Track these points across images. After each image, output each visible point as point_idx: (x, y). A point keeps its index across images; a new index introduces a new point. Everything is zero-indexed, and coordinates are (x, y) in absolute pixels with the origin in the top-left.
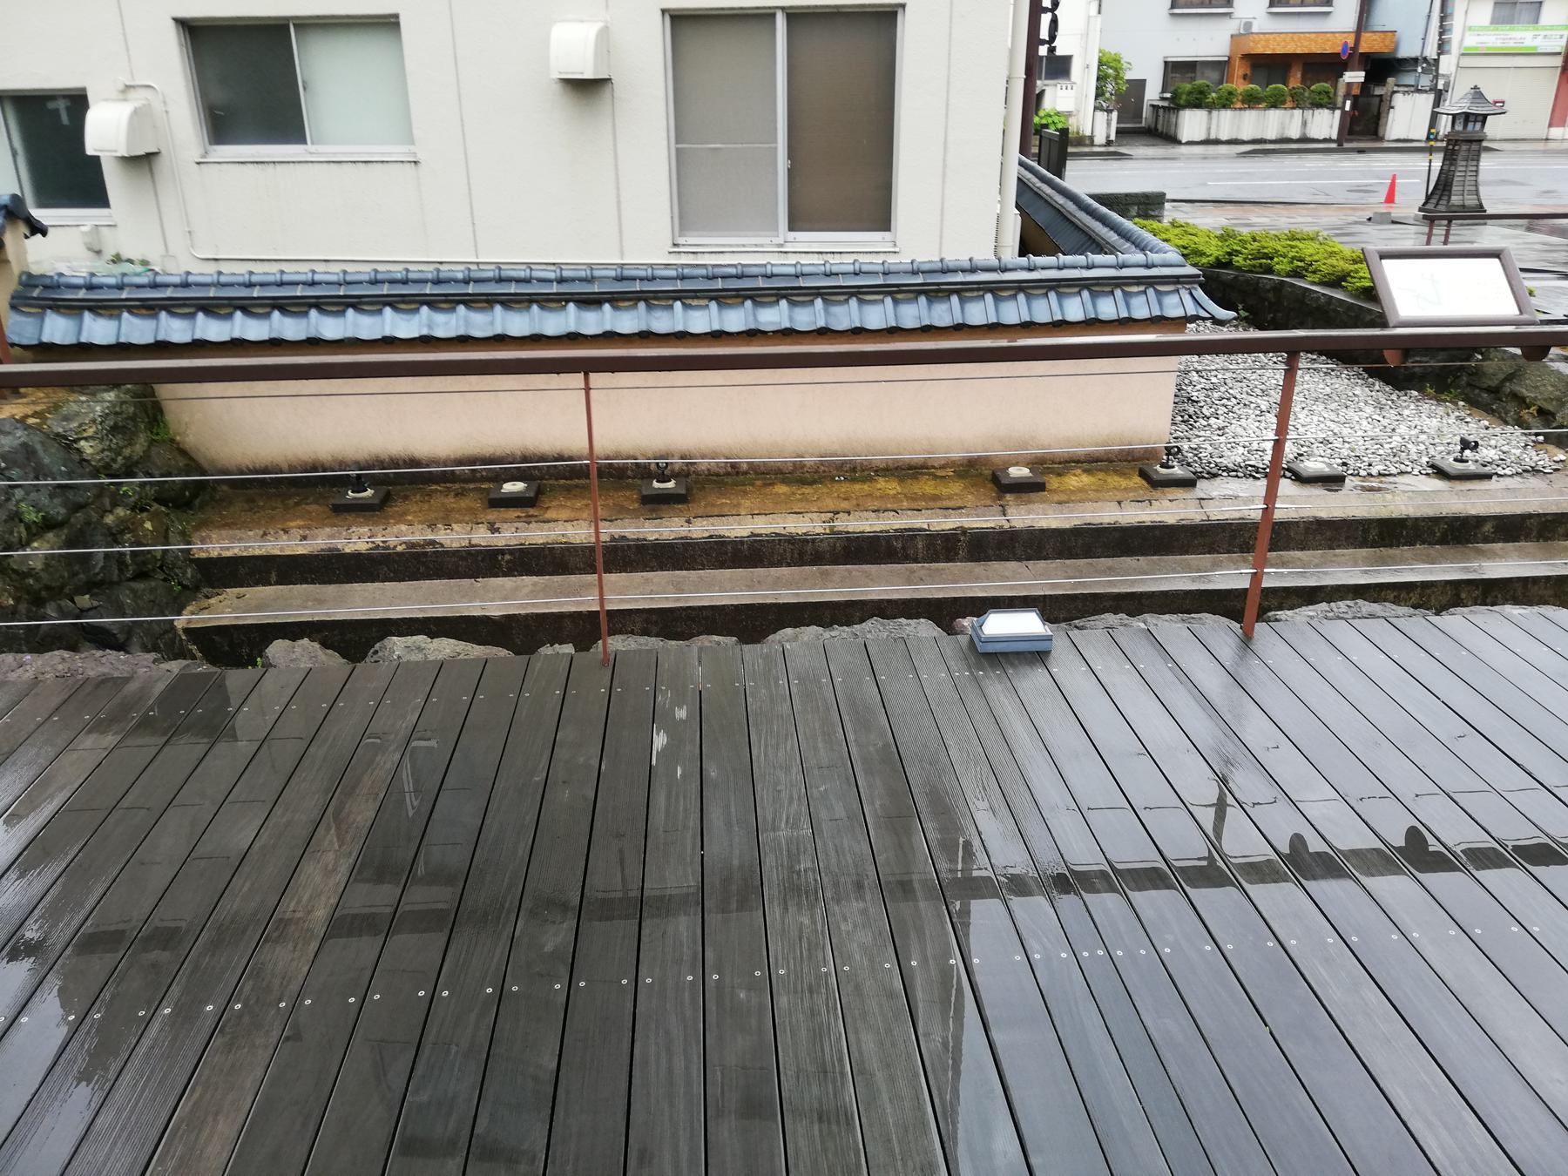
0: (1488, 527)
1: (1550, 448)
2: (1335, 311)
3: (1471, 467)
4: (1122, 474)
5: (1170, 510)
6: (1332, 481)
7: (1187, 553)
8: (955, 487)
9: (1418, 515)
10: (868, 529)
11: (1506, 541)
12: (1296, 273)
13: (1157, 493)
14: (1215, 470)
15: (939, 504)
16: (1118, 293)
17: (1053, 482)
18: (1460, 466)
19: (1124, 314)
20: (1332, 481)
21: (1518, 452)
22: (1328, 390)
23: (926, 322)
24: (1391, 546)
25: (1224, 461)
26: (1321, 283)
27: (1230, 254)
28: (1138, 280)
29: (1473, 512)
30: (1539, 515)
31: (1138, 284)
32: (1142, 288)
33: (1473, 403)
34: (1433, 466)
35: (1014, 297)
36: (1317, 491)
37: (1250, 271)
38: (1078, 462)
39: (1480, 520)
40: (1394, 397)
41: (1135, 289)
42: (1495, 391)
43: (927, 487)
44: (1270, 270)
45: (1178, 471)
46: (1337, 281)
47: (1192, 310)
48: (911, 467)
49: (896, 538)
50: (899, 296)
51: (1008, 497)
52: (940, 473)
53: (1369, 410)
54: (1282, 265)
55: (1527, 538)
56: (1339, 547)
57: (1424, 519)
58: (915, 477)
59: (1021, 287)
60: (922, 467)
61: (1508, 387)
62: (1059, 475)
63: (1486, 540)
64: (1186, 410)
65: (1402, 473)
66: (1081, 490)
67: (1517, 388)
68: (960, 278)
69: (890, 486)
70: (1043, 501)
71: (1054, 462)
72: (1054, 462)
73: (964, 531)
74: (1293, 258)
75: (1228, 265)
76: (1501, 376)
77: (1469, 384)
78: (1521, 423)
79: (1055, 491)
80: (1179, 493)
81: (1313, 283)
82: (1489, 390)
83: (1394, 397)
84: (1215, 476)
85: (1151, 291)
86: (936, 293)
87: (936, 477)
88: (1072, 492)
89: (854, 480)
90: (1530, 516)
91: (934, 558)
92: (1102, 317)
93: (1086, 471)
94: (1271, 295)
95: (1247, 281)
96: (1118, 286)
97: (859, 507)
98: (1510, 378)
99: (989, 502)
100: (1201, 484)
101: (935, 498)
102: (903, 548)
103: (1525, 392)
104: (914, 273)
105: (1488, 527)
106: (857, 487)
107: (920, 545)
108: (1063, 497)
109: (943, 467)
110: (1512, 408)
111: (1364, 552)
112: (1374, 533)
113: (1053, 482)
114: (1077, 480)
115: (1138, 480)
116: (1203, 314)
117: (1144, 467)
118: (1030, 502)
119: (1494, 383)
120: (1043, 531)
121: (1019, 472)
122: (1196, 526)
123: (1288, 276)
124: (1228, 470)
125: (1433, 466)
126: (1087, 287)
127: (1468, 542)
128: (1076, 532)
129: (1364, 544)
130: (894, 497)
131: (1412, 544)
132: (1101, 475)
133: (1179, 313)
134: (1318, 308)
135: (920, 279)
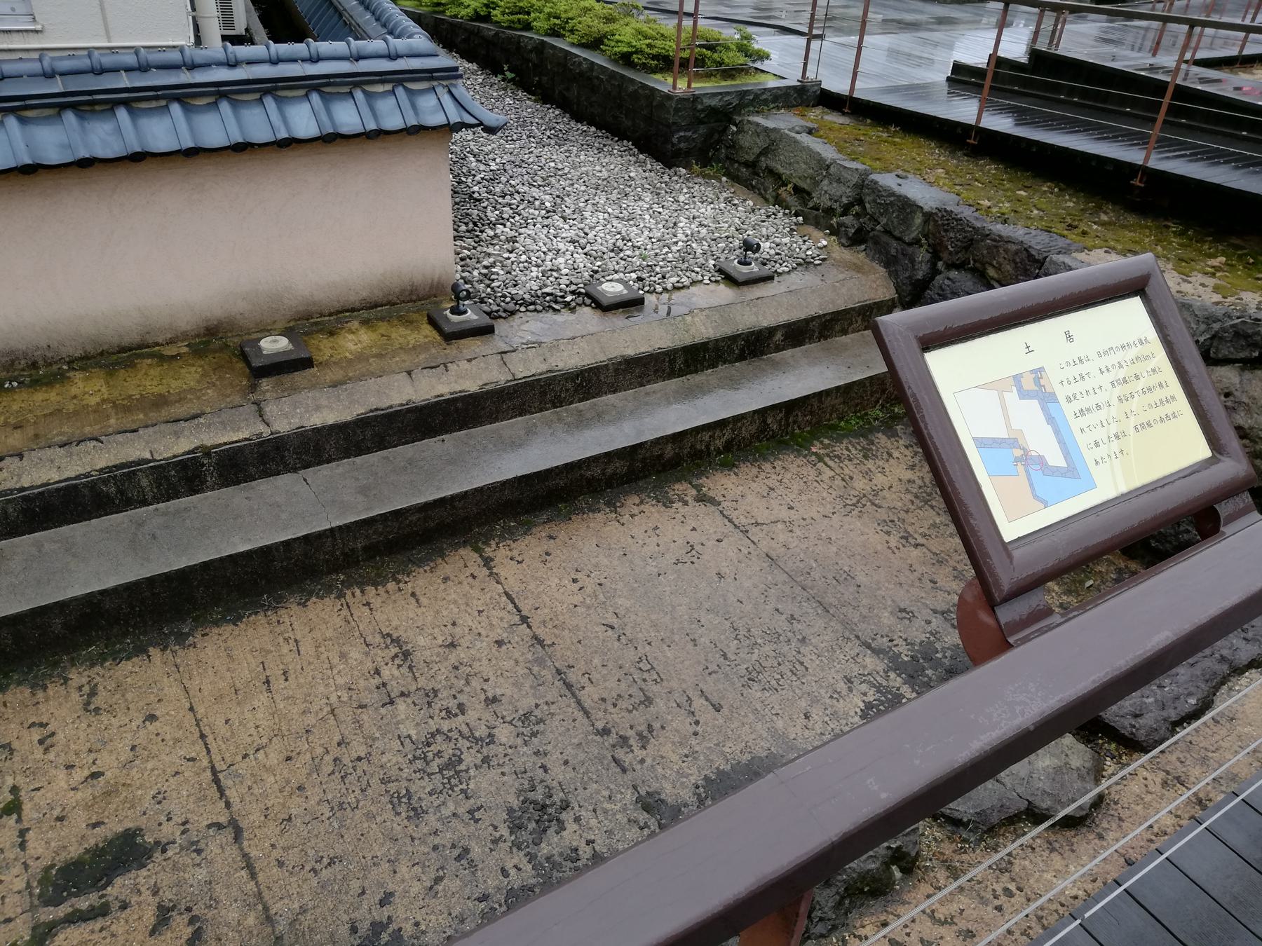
0: (779, 336)
1: (810, 229)
2: (598, 78)
3: (754, 268)
4: (408, 323)
5: (470, 373)
6: (631, 305)
7: (496, 420)
8: (190, 376)
9: (718, 336)
10: (55, 477)
11: (794, 346)
12: (554, 32)
13: (452, 350)
14: (511, 306)
15: (165, 413)
16: (359, 94)
17: (323, 348)
18: (744, 269)
19: (372, 126)
20: (631, 305)
21: (787, 240)
22: (605, 174)
23: (83, 153)
24: (696, 372)
25: (519, 291)
26: (581, 45)
27: (487, 6)
28: (382, 77)
29: (765, 324)
30: (819, 316)
31: (383, 82)
32: (388, 87)
33: (735, 178)
34: (720, 271)
35: (215, 104)
36: (617, 320)
37: (509, 28)
38: (353, 310)
39: (771, 331)
40: (666, 178)
41: (380, 88)
42: (752, 165)
43: (146, 381)
44: (527, 27)
45: (472, 316)
46: (595, 43)
47: (455, 116)
48: (123, 350)
49: (105, 481)
50: (29, 114)
51: (266, 384)
52: (169, 351)
53: (648, 197)
54: (540, 24)
55: (811, 340)
56: (649, 382)
57: (723, 339)
58: (130, 365)
59: (221, 92)
60: (140, 347)
61: (764, 162)
62: (332, 334)
63: (778, 349)
64: (470, 218)
65: (694, 283)
66: (361, 357)
67: (773, 164)
68: (124, 81)
69: (89, 388)
70: (313, 387)
71: (322, 315)
72: (322, 315)
73: (206, 451)
74: (549, 15)
75: (487, 18)
76: (757, 151)
77: (727, 158)
78: (778, 201)
79: (325, 365)
80: (473, 346)
81: (573, 45)
82: (747, 164)
83: (666, 178)
84: (513, 313)
85: (400, 91)
86: (89, 105)
87: (162, 358)
88: (350, 362)
89: (36, 383)
90: (813, 319)
91: (170, 493)
92: (344, 130)
93: (366, 322)
94: (533, 56)
95: (509, 38)
96: (356, 85)
97: (39, 441)
98: (765, 152)
99: (237, 399)
100: (501, 327)
101: (160, 401)
102: (121, 492)
103: (781, 170)
104: (49, 75)
105: (779, 336)
106: (39, 396)
107: (145, 482)
108: (337, 374)
109: (171, 342)
110: (770, 183)
111: (674, 383)
112: (679, 362)
113: (323, 348)
114: (355, 341)
115: (427, 330)
116: (469, 120)
117: (435, 311)
118: (294, 389)
119: (751, 158)
120: (317, 430)
121: (274, 345)
122: (502, 390)
123: (547, 35)
124: (525, 303)
125: (720, 271)
126: (316, 88)
127: (763, 353)
128: (361, 423)
129: (672, 374)
130: (97, 409)
131: (714, 366)
132: (383, 327)
133: (439, 119)
134: (581, 74)
135: (57, 86)
